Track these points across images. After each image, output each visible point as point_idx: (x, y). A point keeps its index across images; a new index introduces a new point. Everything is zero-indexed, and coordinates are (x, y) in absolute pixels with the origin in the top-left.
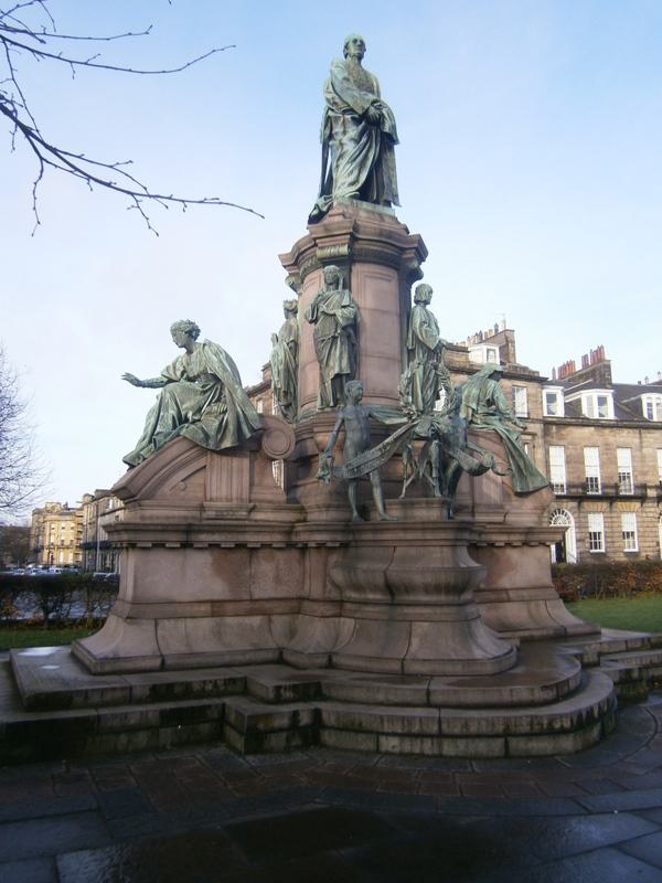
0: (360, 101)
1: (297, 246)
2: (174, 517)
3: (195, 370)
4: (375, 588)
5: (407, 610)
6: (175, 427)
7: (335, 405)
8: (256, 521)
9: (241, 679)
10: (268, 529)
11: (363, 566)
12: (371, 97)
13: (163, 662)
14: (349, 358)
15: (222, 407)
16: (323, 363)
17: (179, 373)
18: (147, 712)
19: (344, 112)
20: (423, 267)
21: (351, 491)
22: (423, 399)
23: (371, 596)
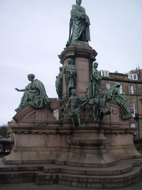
0: (80, 14)
1: (62, 53)
2: (27, 125)
3: (33, 87)
4: (77, 145)
5: (85, 150)
6: (27, 102)
7: (70, 96)
8: (49, 126)
9: (41, 167)
10: (51, 129)
11: (75, 139)
12: (82, 14)
13: (23, 162)
14: (74, 83)
15: (39, 96)
16: (67, 85)
17: (29, 88)
18: (16, 174)
19: (75, 18)
20: (96, 58)
21: (72, 119)
22: (95, 94)
23: (77, 147)
